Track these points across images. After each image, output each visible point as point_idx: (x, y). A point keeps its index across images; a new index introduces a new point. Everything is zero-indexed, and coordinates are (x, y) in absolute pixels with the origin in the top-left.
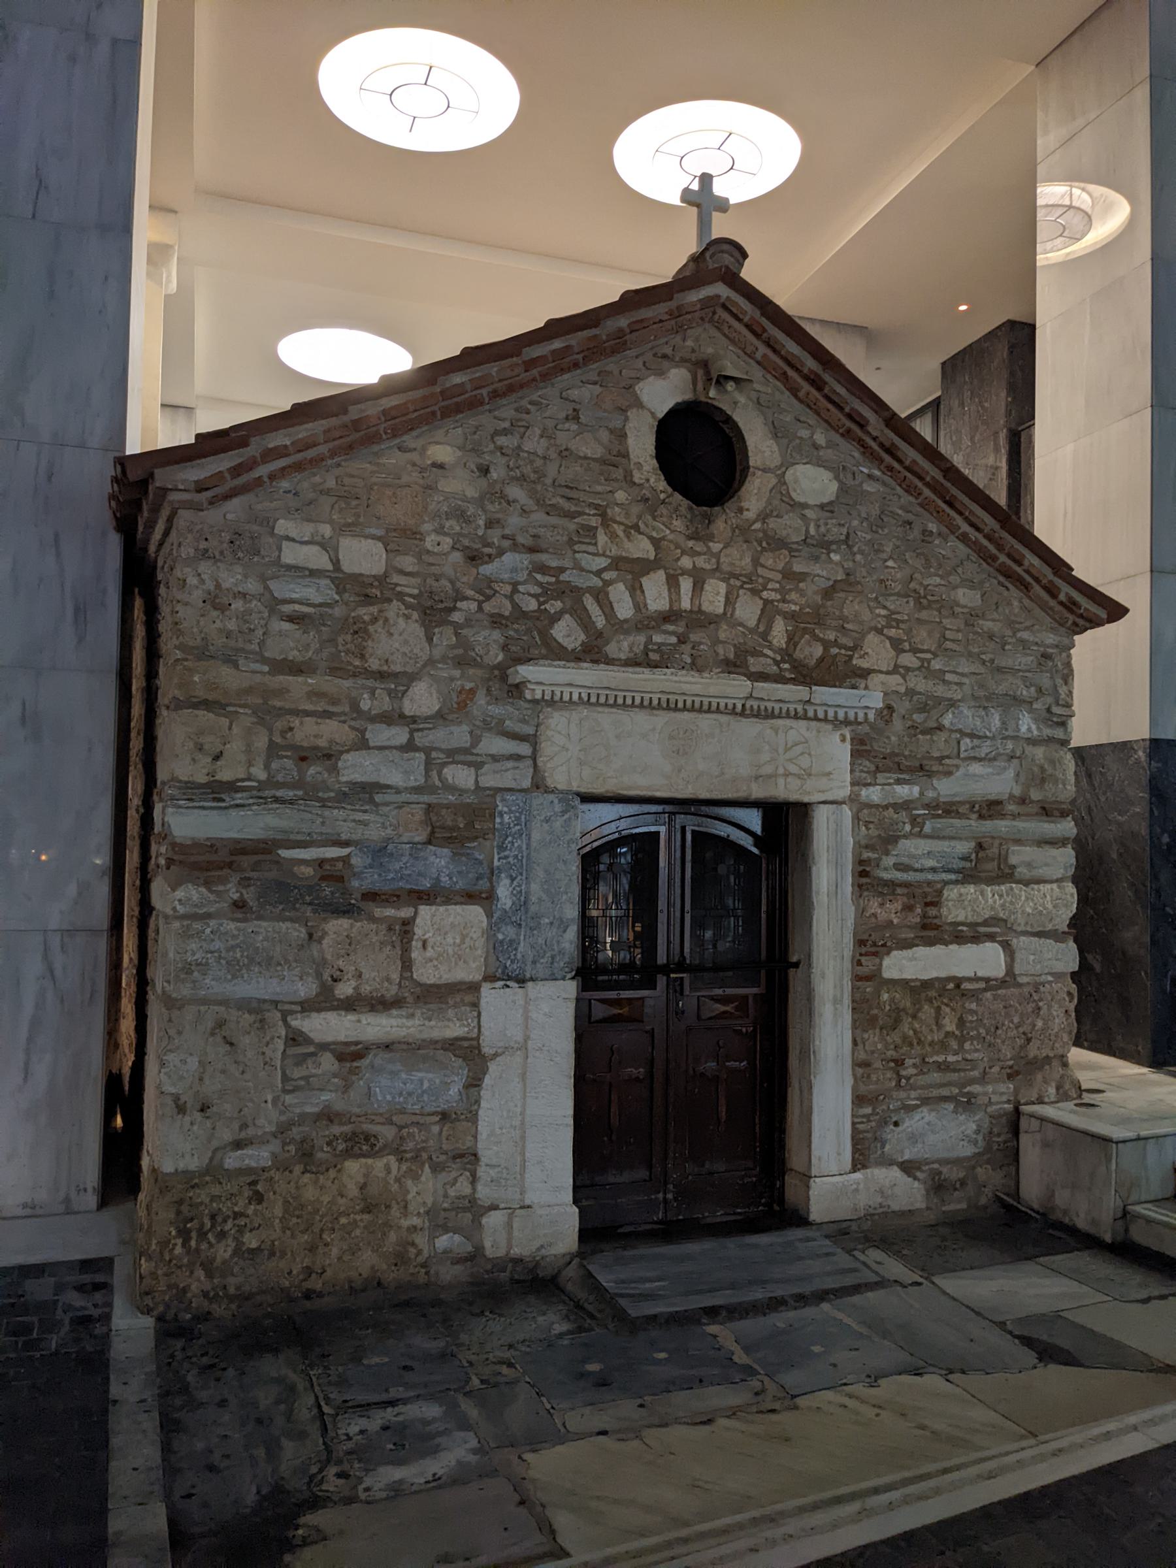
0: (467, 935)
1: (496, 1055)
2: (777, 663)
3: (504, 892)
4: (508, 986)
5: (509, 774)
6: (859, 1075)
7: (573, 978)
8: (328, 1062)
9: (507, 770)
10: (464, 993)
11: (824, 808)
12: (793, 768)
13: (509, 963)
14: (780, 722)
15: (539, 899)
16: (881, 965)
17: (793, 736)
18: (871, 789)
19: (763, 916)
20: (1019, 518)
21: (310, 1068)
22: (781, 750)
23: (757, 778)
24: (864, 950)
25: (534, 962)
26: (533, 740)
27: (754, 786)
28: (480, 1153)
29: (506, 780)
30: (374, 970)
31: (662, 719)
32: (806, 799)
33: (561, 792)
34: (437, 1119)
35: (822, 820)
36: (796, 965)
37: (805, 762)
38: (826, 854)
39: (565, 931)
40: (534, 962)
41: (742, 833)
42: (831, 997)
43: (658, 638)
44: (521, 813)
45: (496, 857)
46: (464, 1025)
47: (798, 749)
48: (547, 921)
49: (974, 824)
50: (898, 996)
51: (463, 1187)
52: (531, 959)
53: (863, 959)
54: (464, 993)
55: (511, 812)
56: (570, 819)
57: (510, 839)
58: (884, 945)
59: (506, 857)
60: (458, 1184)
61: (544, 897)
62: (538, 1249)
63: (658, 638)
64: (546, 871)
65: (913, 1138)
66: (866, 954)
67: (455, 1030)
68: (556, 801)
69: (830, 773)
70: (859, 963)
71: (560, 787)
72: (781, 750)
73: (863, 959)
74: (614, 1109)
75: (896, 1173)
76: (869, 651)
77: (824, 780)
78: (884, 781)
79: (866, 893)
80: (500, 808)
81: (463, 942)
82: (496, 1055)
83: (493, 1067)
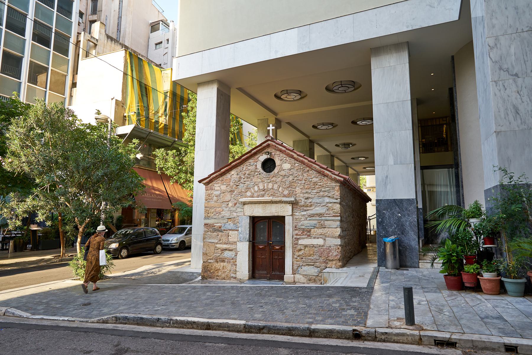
3: (240, 229)
8: (219, 250)
10: (235, 243)
19: (9, 268)
20: (127, 134)
21: (218, 251)
30: (224, 239)
35: (286, 218)
49: (318, 218)
54: (235, 243)
65: (304, 271)
75: (301, 276)
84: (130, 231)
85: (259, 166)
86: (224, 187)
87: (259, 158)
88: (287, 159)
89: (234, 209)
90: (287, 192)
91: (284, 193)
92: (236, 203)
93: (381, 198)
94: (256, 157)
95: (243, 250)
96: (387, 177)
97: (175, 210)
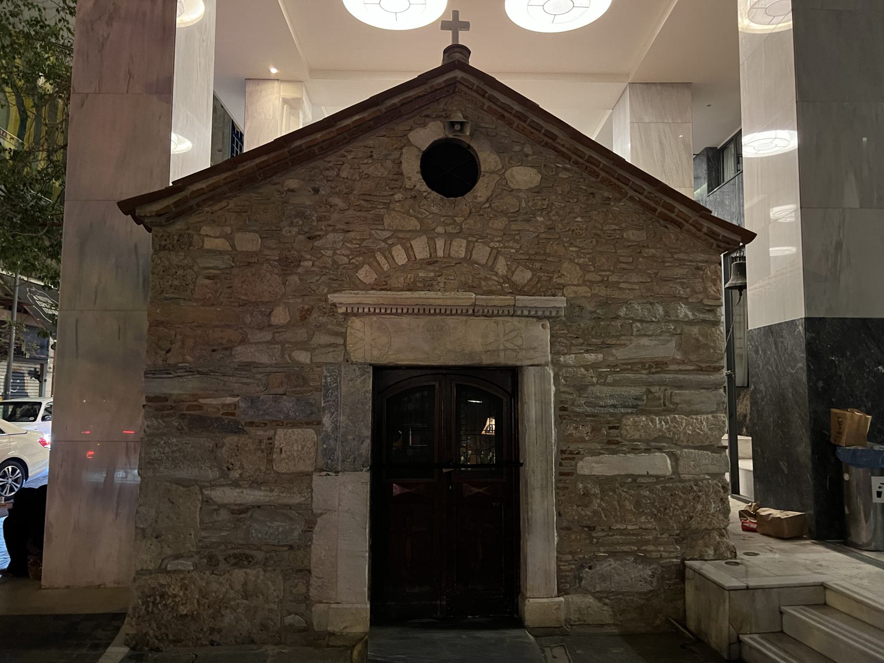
1: (321, 514)
2: (501, 284)
5: (330, 355)
8: (224, 515)
12: (509, 345)
16: (576, 465)
18: (568, 357)
23: (486, 352)
24: (564, 456)
26: (344, 336)
27: (484, 357)
29: (330, 358)
31: (423, 321)
32: (519, 364)
33: (361, 364)
47: (514, 334)
49: (643, 376)
51: (302, 589)
53: (563, 462)
55: (331, 376)
59: (328, 401)
62: (344, 628)
63: (421, 275)
65: (603, 578)
67: (297, 499)
68: (357, 369)
70: (561, 465)
71: (359, 361)
73: (563, 462)
75: (590, 599)
77: (532, 352)
82: (321, 514)
84: (26, 279)
85: (412, 167)
86: (249, 242)
87: (412, 136)
88: (528, 149)
89: (301, 334)
90: (528, 275)
91: (514, 278)
92: (309, 311)
93: (820, 313)
94: (401, 127)
95: (345, 503)
96: (839, 246)
97: (738, 637)
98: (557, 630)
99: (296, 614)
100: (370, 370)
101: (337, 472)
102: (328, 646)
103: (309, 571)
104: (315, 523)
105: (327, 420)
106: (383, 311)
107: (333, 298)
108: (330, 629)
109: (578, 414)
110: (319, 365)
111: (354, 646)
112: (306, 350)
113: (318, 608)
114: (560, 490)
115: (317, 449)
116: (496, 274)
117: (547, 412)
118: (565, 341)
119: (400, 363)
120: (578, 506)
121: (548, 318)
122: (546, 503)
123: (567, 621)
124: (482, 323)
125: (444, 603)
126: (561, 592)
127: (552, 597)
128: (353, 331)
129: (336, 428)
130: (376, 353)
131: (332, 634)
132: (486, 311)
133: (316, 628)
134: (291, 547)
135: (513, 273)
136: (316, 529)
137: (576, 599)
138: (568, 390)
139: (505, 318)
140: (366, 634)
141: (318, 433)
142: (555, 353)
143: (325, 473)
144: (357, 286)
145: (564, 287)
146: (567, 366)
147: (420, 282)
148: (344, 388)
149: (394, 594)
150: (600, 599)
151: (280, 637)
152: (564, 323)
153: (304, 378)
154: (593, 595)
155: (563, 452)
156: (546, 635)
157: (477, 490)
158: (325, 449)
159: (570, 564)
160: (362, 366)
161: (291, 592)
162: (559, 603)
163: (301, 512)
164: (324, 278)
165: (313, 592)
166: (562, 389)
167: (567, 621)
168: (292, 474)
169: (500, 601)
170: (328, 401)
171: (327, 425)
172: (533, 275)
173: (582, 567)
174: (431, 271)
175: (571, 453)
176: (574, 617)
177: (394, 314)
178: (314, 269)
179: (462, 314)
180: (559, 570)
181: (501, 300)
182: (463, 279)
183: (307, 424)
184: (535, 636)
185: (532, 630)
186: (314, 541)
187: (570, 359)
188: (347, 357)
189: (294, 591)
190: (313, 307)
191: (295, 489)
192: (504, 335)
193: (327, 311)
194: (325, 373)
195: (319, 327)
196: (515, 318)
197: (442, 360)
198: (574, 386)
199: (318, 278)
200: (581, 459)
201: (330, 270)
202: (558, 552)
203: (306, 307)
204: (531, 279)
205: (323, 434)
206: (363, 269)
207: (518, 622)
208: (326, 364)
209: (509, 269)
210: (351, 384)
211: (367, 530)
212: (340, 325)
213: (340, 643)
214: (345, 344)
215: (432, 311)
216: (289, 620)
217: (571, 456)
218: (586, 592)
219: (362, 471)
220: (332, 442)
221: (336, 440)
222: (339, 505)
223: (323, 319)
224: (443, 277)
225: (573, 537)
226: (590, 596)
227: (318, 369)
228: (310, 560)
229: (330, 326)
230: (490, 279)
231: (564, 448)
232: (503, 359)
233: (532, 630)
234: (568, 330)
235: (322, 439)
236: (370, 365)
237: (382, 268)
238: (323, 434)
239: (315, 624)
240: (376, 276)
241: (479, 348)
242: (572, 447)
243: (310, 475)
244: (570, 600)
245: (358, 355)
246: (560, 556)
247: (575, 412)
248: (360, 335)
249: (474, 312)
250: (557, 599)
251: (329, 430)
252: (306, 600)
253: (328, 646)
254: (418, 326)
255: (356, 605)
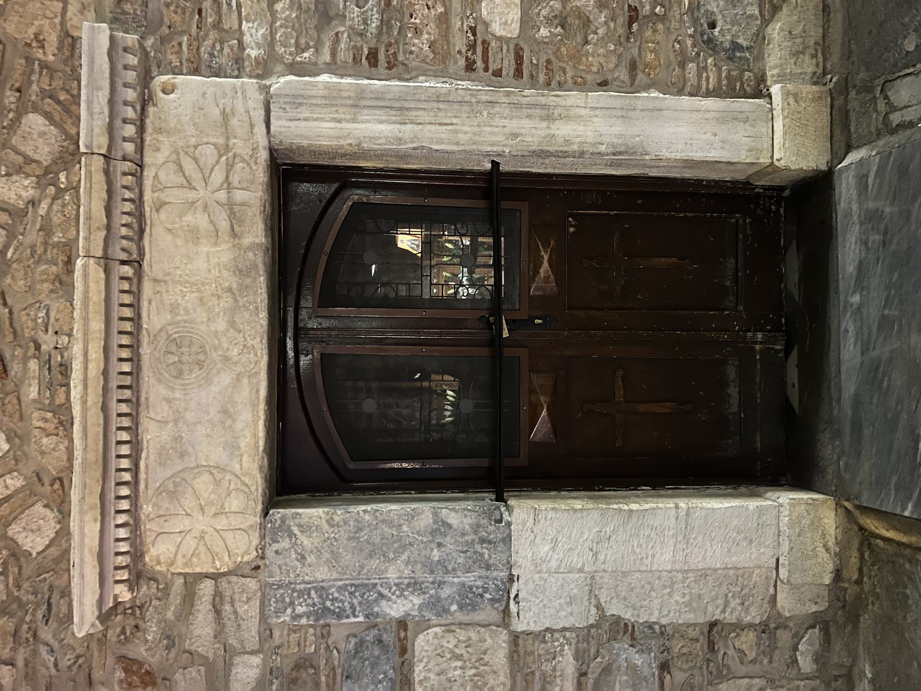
0: (451, 651)
1: (598, 607)
2: (60, 193)
4: (517, 596)
5: (242, 609)
6: (646, 80)
7: (509, 509)
9: (235, 612)
11: (275, 124)
12: (218, 177)
13: (488, 596)
14: (148, 196)
15: (407, 563)
16: (499, 39)
17: (168, 176)
18: (247, 39)
22: (191, 195)
23: (234, 234)
24: (479, 64)
25: (488, 567)
26: (192, 581)
27: (247, 240)
28: (708, 618)
29: (250, 611)
31: (153, 388)
32: (264, 155)
33: (263, 537)
34: (668, 677)
36: (495, 164)
37: (208, 154)
38: (344, 125)
39: (449, 526)
40: (488, 567)
41: (305, 394)
42: (544, 124)
43: (33, 392)
44: (294, 591)
45: (353, 620)
46: (562, 650)
47: (189, 165)
48: (435, 552)
50: (543, 12)
51: (747, 641)
52: (483, 573)
53: (493, 67)
55: (292, 604)
56: (300, 526)
57: (328, 603)
58: (473, 30)
59: (353, 607)
60: (744, 647)
61: (404, 557)
62: (827, 550)
63: (33, 392)
64: (371, 556)
66: (486, 61)
67: (568, 663)
68: (275, 546)
69: (224, 113)
70: (498, 73)
71: (255, 542)
72: (191, 195)
73: (493, 67)
74: (654, 408)
75: (775, 30)
76: (31, 31)
77: (234, 122)
78: (235, 15)
79: (401, 58)
80: (287, 619)
81: (458, 657)
82: (598, 607)
83: (614, 609)
90: (35, 122)
98: (836, 103)
99: (795, 648)
100: (277, 514)
101: (511, 579)
102: (859, 582)
103: (713, 625)
104: (617, 620)
105: (395, 609)
106: (124, 491)
107: (85, 618)
108: (827, 580)
109: (385, 24)
110: (267, 632)
111: (861, 529)
112: (228, 666)
113: (786, 603)
114: (552, 81)
115: (461, 624)
116: (33, 203)
117: (379, 96)
118: (208, 42)
119: (261, 443)
120: (587, 42)
121: (146, 79)
122: (582, 112)
123: (817, 79)
124: (161, 246)
125: (760, 336)
126: (760, 91)
127: (772, 110)
128: (180, 561)
129: (415, 586)
130: (235, 503)
131: (838, 575)
132: (124, 231)
133: (822, 606)
134: (664, 667)
135: (29, 160)
136: (628, 615)
137: (775, 58)
138: (328, 44)
139: (148, 183)
140: (838, 505)
141: (424, 625)
142: (238, 67)
143: (513, 607)
144: (59, 558)
145: (68, 35)
146: (271, 44)
147: (52, 397)
148: (323, 574)
149: (751, 442)
150: (776, 9)
151: (836, 678)
152: (163, 40)
153: (297, 667)
154: (766, 22)
155: (470, 67)
156: (846, 125)
157: (546, 264)
158: (461, 607)
159: (705, 68)
160: (267, 533)
161: (753, 662)
162: (786, 94)
163: (593, 651)
164: (46, 634)
165: (754, 616)
166: (327, 57)
167: (817, 79)
168: (513, 677)
169: (780, 219)
170: (353, 607)
171: (408, 606)
172: (36, 109)
173: (710, 41)
174: (26, 369)
175: (472, 47)
176: (809, 66)
177: (136, 465)
178: (20, 663)
179: (137, 294)
180: (715, 93)
181: (90, 191)
182: (47, 286)
183: (403, 651)
184: (849, 149)
185: (837, 155)
186: (653, 619)
187: (254, 34)
188: (247, 571)
189: (751, 655)
190: (121, 658)
191: (547, 667)
192: (193, 188)
193: (131, 622)
194: (286, 618)
195: (170, 639)
196: (147, 160)
197: (258, 346)
198: (319, 29)
199: (43, 650)
200: (487, 25)
201: (22, 620)
202: (680, 92)
203: (120, 674)
204: (48, 116)
205: (427, 615)
206: (20, 539)
207: (814, 190)
208: (263, 617)
209: (19, 170)
210: (311, 559)
211: (634, 507)
212: (166, 591)
213: (854, 560)
214: (215, 577)
215: (126, 367)
216: (806, 663)
217: (479, 50)
218: (760, 38)
219: (509, 524)
220: (446, 592)
221: (441, 584)
222: (581, 571)
223: (152, 631)
224: (42, 337)
225: (650, 57)
226: (769, 28)
227: (276, 634)
228: (689, 625)
229: (170, 615)
230: (47, 218)
231: (462, 62)
232: (253, 194)
233: (837, 155)
234: (183, 32)
235: (439, 615)
236: (266, 514)
237: (17, 492)
238: (427, 615)
239: (814, 608)
240: (39, 508)
241: (224, 253)
242: (459, 43)
243: (515, 638)
244: (775, 72)
245: (242, 546)
246: (688, 89)
247: (380, 28)
248: (190, 543)
249: (128, 262)
250: (777, 98)
251: (417, 601)
252: (767, 630)
253: (859, 582)
254: (169, 401)
255: (783, 528)
